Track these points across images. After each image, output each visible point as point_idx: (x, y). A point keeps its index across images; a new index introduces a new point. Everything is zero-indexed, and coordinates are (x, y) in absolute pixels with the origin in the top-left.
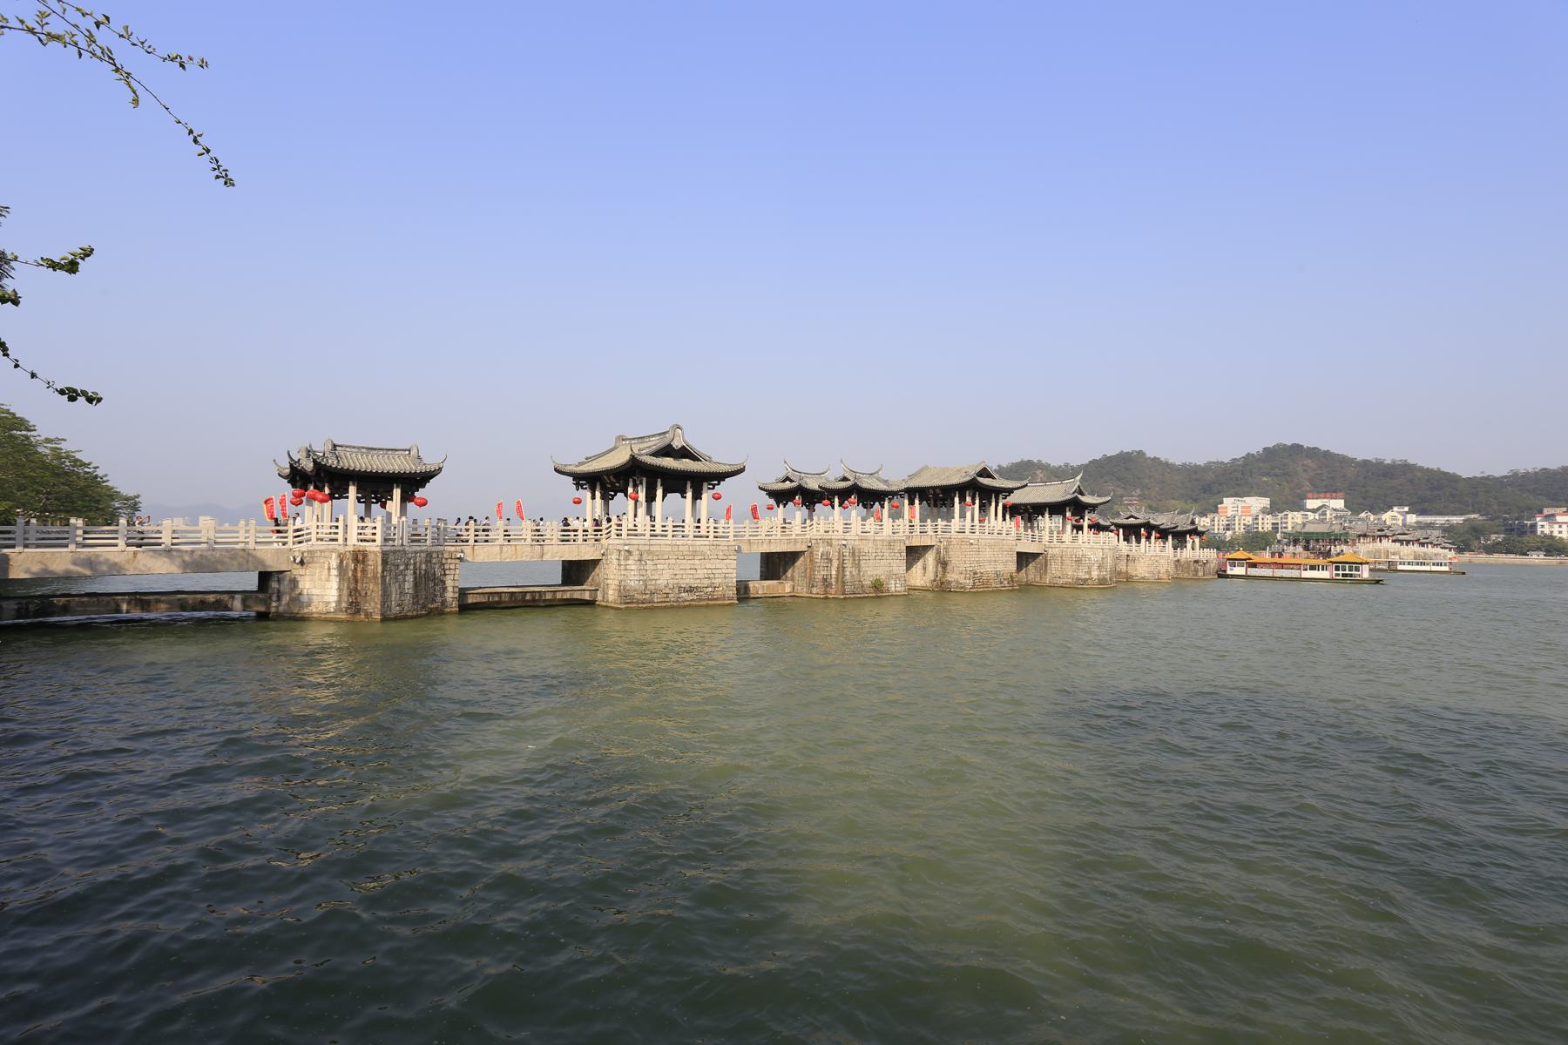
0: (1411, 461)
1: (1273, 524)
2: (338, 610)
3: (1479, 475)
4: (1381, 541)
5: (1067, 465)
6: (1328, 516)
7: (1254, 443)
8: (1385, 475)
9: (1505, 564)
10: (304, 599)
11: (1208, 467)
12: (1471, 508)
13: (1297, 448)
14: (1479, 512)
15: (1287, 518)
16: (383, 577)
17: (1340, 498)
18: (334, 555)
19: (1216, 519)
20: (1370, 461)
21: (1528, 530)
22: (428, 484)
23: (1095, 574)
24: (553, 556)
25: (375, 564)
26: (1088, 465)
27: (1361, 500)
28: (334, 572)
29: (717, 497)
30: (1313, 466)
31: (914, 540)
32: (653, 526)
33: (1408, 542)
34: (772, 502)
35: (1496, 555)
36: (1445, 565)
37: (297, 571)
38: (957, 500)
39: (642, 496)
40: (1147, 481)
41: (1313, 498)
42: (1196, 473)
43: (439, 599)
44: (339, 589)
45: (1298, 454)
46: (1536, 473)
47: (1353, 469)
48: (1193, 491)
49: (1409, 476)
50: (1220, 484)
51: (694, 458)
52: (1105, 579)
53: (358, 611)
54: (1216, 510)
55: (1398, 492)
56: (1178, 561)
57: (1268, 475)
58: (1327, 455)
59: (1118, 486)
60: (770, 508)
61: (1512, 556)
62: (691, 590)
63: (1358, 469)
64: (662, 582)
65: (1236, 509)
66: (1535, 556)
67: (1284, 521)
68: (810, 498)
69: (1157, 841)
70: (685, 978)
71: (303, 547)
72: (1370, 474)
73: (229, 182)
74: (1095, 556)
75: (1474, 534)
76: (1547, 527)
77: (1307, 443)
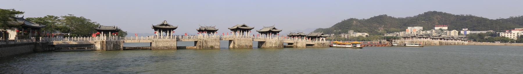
0: (473, 15)
2: (100, 49)
3: (499, 19)
4: (428, 38)
5: (364, 19)
6: (433, 32)
8: (463, 19)
9: (486, 45)
11: (407, 18)
12: (490, 28)
13: (435, 12)
14: (493, 30)
16: (106, 45)
20: (459, 15)
21: (497, 35)
22: (372, 17)
23: (274, 45)
25: (105, 43)
26: (370, 19)
27: (454, 27)
29: (174, 32)
30: (440, 17)
32: (511, 36)
33: (437, 39)
34: (198, 32)
35: (484, 43)
36: (418, 44)
37: (95, 44)
38: (168, 32)
39: (239, 32)
40: (386, 23)
41: (437, 27)
42: (402, 20)
46: (519, 18)
48: (401, 25)
49: (471, 19)
51: (276, 29)
54: (405, 31)
55: (467, 24)
57: (424, 20)
58: (445, 14)
59: (377, 24)
60: (198, 33)
62: (166, 47)
63: (454, 18)
64: (160, 46)
66: (497, 43)
68: (294, 36)
70: (3, 35)
71: (96, 40)
72: (458, 19)
74: (274, 42)
75: (479, 36)
77: (438, 10)
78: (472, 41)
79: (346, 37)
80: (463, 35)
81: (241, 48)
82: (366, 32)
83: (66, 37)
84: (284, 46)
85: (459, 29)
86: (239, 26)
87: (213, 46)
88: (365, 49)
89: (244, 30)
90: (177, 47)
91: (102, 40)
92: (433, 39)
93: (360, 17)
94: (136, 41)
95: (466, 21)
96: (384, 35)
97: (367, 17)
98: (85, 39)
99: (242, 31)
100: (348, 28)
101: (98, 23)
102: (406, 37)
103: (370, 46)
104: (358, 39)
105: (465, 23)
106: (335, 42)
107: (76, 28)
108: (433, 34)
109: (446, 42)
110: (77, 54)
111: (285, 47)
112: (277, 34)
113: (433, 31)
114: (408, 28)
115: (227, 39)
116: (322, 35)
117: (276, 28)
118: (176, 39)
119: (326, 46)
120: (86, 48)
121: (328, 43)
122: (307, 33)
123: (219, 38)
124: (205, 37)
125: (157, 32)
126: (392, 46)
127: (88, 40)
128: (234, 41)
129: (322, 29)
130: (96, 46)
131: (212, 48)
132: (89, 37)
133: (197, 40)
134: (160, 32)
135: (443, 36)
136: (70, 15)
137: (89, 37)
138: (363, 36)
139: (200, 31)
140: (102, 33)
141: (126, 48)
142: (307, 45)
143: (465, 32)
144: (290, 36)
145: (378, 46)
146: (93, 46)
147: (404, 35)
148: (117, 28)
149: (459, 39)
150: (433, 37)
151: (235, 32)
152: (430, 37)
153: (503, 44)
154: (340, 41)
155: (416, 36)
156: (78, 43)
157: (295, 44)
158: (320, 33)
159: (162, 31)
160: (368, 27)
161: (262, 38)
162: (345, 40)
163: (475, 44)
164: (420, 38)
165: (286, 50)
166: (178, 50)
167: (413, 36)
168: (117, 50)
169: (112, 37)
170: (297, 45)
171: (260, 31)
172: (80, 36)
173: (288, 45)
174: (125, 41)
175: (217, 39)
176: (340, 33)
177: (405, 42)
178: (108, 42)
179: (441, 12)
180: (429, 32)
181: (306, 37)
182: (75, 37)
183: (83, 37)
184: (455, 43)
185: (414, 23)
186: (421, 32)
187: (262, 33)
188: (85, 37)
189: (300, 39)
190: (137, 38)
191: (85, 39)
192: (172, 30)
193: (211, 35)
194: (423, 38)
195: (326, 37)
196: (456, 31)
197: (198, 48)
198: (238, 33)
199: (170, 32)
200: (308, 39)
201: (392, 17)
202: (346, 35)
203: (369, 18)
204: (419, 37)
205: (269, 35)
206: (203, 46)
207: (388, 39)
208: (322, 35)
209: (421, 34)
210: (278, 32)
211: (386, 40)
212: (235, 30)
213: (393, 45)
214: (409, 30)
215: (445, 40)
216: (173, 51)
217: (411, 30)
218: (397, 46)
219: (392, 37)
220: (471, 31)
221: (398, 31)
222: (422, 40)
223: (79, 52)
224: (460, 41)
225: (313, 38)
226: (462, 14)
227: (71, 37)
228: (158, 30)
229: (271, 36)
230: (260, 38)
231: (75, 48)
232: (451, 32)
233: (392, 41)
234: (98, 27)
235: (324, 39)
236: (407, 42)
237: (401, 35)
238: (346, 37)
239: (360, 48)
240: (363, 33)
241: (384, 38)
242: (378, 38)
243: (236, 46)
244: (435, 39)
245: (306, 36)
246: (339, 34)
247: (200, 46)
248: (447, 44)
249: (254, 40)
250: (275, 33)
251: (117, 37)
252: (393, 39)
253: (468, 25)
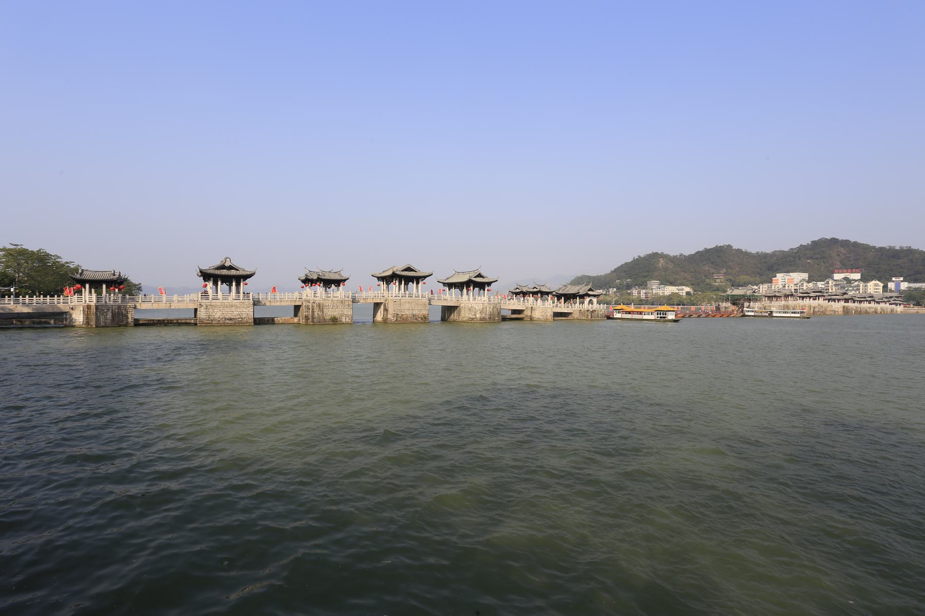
0: (914, 247)
1: (795, 289)
2: (83, 324)
4: (819, 299)
5: (681, 255)
6: (830, 284)
7: (806, 239)
8: (893, 257)
10: (74, 320)
11: (774, 254)
13: (834, 241)
15: (803, 286)
18: (81, 307)
20: (885, 248)
23: (478, 316)
24: (175, 307)
25: (93, 310)
26: (694, 254)
27: (874, 273)
28: (82, 312)
29: (246, 284)
31: (368, 300)
33: (839, 300)
34: (303, 285)
36: (798, 313)
37: (71, 312)
38: (234, 284)
39: (397, 283)
40: (730, 264)
41: (839, 273)
43: (125, 322)
44: (83, 318)
45: (834, 245)
47: (872, 253)
48: (761, 270)
50: (779, 265)
51: (483, 277)
52: (485, 319)
53: (89, 325)
54: (771, 282)
55: (901, 268)
56: (580, 310)
57: (811, 258)
58: (856, 244)
59: (711, 267)
60: (303, 287)
61: (174, 457)
62: (231, 319)
63: (875, 253)
64: (217, 316)
65: (784, 280)
67: (801, 287)
68: (524, 294)
77: (841, 237)
78: (912, 305)
79: (643, 296)
80: (893, 291)
81: (402, 321)
82: (687, 286)
83: (7, 297)
84: (502, 316)
85: (885, 278)
86: (397, 270)
87: (337, 316)
88: (684, 323)
89: (408, 280)
90: (255, 319)
91: (87, 302)
92: (829, 300)
93: (673, 251)
94: (162, 306)
95: (900, 261)
96: (725, 292)
97: (689, 251)
98: (48, 301)
99: (403, 282)
100: (648, 276)
101: (76, 263)
102: (772, 296)
103: (695, 315)
104: (670, 300)
105: (897, 265)
106: (619, 307)
107: (28, 275)
108: (830, 289)
109: (856, 307)
110: (27, 334)
111: (504, 319)
112: (486, 289)
113: (830, 282)
114: (778, 275)
115: (369, 301)
116: (590, 290)
117: (483, 274)
118: (251, 301)
119: (598, 317)
120: (52, 322)
121: (602, 309)
122: (554, 287)
123: (350, 299)
124: (318, 295)
125: (210, 284)
126: (744, 316)
127: (56, 302)
128: (385, 306)
129: (589, 277)
130: (74, 316)
131: (335, 321)
132: (58, 297)
133: (300, 304)
134: (215, 283)
135: (851, 293)
136: (15, 245)
137: (59, 296)
138: (681, 294)
139: (307, 281)
140: (87, 286)
141: (141, 322)
142: (557, 315)
143: (898, 285)
144: (517, 294)
145: (713, 317)
146: (68, 317)
147: (768, 292)
148: (120, 275)
149: (884, 302)
150: (829, 295)
151: (388, 284)
152: (824, 296)
154: (630, 304)
155: (794, 294)
156: (33, 309)
157: (528, 313)
158: (586, 285)
159: (219, 283)
161: (451, 297)
162: (641, 302)
163: (917, 312)
165: (507, 325)
166: (256, 326)
167: (788, 293)
168: (120, 326)
169: (110, 295)
170: (534, 316)
171: (446, 282)
172: (37, 294)
173: (512, 314)
174: (138, 307)
175: (345, 301)
176: (629, 287)
177: (770, 306)
178: (100, 307)
179: (846, 241)
180: (821, 285)
181: (553, 295)
182: (27, 296)
183: (45, 296)
184: (876, 309)
185: (791, 265)
186: (805, 284)
187: (451, 285)
188: (48, 296)
189: (539, 299)
190: (164, 297)
191: (48, 301)
192: (242, 280)
193: (333, 290)
194: (810, 297)
195: (599, 295)
196: (877, 282)
197: (302, 321)
198: (394, 286)
199: (238, 285)
200: (558, 300)
201: (743, 250)
202: (642, 292)
203: (693, 253)
204: (800, 297)
205: (468, 290)
206: (313, 318)
207: (735, 301)
208: (589, 290)
209: (805, 289)
210: (489, 284)
211: (731, 303)
212: (388, 280)
213: (746, 314)
214: (780, 281)
215: (854, 302)
216: (243, 330)
217: (784, 281)
218: (754, 316)
219: (743, 296)
220: (909, 282)
221: (756, 282)
222: (807, 302)
223: (27, 329)
224: (888, 305)
225: (569, 297)
226: (891, 245)
227: (17, 295)
228: (212, 279)
229: (472, 293)
230: (446, 297)
231: (27, 323)
232: (869, 284)
233: (743, 305)
234: (77, 273)
235: (595, 300)
236: (775, 307)
237: (761, 291)
238: (643, 296)
239: (675, 321)
240: (680, 288)
241: (727, 300)
242: (713, 298)
243: (389, 316)
244: (835, 301)
245: (554, 293)
246: (627, 289)
247: (307, 318)
248: (859, 312)
249: (433, 302)
250: (482, 286)
251: (120, 295)
252: (745, 300)
253: (904, 270)
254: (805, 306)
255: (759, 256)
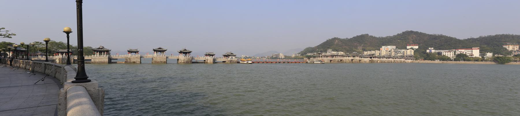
5: (347, 38)
6: (392, 51)
8: (434, 39)
11: (387, 38)
13: (412, 32)
17: (417, 46)
19: (376, 52)
23: (182, 62)
25: (61, 59)
33: (367, 57)
35: (426, 61)
38: (103, 53)
41: (409, 46)
57: (400, 39)
58: (421, 34)
61: (430, 61)
62: (101, 62)
69: (404, 53)
73: (15, 35)
76: (444, 53)
82: (342, 51)
88: (253, 64)
93: (343, 36)
95: (437, 41)
97: (350, 36)
114: (383, 47)
119: (233, 62)
126: (307, 63)
131: (134, 62)
134: (157, 52)
153: (441, 62)
160: (349, 46)
164: (346, 56)
194: (385, 58)
199: (163, 52)
201: (373, 36)
217: (385, 50)
220: (436, 50)
254: (346, 59)
255: (380, 39)
